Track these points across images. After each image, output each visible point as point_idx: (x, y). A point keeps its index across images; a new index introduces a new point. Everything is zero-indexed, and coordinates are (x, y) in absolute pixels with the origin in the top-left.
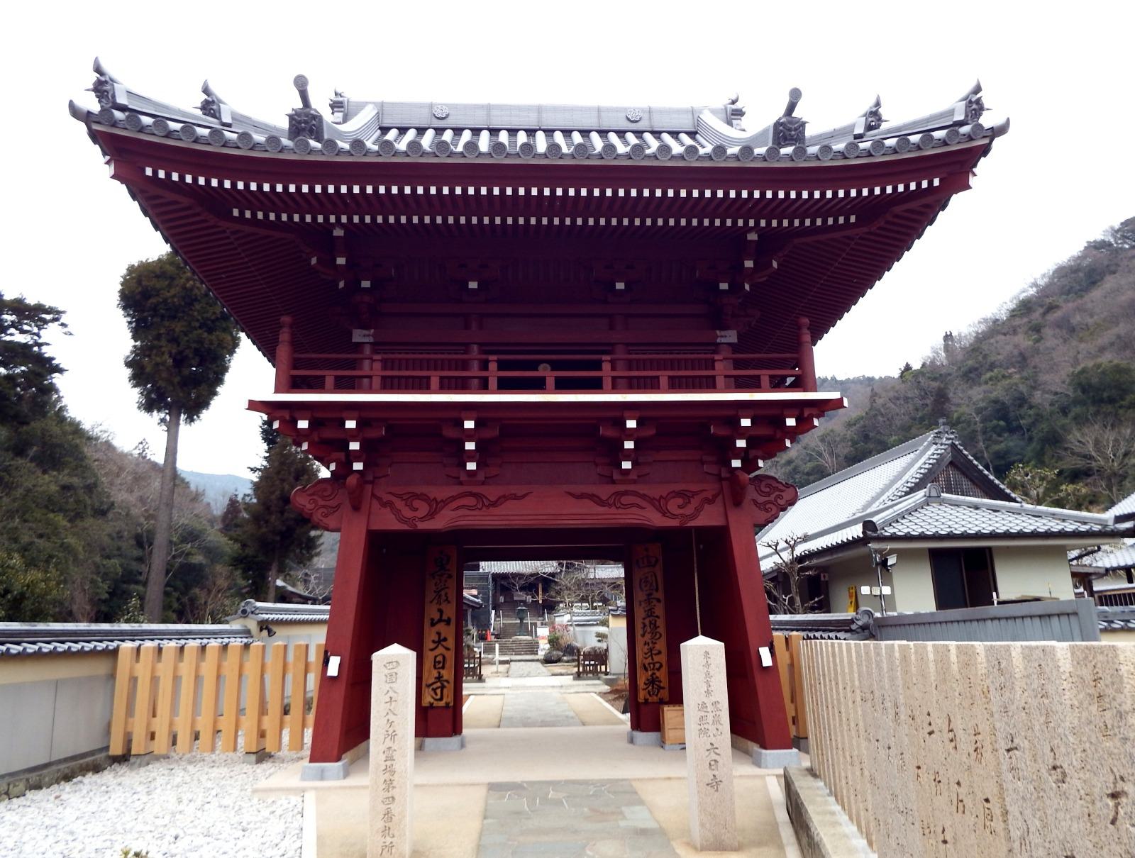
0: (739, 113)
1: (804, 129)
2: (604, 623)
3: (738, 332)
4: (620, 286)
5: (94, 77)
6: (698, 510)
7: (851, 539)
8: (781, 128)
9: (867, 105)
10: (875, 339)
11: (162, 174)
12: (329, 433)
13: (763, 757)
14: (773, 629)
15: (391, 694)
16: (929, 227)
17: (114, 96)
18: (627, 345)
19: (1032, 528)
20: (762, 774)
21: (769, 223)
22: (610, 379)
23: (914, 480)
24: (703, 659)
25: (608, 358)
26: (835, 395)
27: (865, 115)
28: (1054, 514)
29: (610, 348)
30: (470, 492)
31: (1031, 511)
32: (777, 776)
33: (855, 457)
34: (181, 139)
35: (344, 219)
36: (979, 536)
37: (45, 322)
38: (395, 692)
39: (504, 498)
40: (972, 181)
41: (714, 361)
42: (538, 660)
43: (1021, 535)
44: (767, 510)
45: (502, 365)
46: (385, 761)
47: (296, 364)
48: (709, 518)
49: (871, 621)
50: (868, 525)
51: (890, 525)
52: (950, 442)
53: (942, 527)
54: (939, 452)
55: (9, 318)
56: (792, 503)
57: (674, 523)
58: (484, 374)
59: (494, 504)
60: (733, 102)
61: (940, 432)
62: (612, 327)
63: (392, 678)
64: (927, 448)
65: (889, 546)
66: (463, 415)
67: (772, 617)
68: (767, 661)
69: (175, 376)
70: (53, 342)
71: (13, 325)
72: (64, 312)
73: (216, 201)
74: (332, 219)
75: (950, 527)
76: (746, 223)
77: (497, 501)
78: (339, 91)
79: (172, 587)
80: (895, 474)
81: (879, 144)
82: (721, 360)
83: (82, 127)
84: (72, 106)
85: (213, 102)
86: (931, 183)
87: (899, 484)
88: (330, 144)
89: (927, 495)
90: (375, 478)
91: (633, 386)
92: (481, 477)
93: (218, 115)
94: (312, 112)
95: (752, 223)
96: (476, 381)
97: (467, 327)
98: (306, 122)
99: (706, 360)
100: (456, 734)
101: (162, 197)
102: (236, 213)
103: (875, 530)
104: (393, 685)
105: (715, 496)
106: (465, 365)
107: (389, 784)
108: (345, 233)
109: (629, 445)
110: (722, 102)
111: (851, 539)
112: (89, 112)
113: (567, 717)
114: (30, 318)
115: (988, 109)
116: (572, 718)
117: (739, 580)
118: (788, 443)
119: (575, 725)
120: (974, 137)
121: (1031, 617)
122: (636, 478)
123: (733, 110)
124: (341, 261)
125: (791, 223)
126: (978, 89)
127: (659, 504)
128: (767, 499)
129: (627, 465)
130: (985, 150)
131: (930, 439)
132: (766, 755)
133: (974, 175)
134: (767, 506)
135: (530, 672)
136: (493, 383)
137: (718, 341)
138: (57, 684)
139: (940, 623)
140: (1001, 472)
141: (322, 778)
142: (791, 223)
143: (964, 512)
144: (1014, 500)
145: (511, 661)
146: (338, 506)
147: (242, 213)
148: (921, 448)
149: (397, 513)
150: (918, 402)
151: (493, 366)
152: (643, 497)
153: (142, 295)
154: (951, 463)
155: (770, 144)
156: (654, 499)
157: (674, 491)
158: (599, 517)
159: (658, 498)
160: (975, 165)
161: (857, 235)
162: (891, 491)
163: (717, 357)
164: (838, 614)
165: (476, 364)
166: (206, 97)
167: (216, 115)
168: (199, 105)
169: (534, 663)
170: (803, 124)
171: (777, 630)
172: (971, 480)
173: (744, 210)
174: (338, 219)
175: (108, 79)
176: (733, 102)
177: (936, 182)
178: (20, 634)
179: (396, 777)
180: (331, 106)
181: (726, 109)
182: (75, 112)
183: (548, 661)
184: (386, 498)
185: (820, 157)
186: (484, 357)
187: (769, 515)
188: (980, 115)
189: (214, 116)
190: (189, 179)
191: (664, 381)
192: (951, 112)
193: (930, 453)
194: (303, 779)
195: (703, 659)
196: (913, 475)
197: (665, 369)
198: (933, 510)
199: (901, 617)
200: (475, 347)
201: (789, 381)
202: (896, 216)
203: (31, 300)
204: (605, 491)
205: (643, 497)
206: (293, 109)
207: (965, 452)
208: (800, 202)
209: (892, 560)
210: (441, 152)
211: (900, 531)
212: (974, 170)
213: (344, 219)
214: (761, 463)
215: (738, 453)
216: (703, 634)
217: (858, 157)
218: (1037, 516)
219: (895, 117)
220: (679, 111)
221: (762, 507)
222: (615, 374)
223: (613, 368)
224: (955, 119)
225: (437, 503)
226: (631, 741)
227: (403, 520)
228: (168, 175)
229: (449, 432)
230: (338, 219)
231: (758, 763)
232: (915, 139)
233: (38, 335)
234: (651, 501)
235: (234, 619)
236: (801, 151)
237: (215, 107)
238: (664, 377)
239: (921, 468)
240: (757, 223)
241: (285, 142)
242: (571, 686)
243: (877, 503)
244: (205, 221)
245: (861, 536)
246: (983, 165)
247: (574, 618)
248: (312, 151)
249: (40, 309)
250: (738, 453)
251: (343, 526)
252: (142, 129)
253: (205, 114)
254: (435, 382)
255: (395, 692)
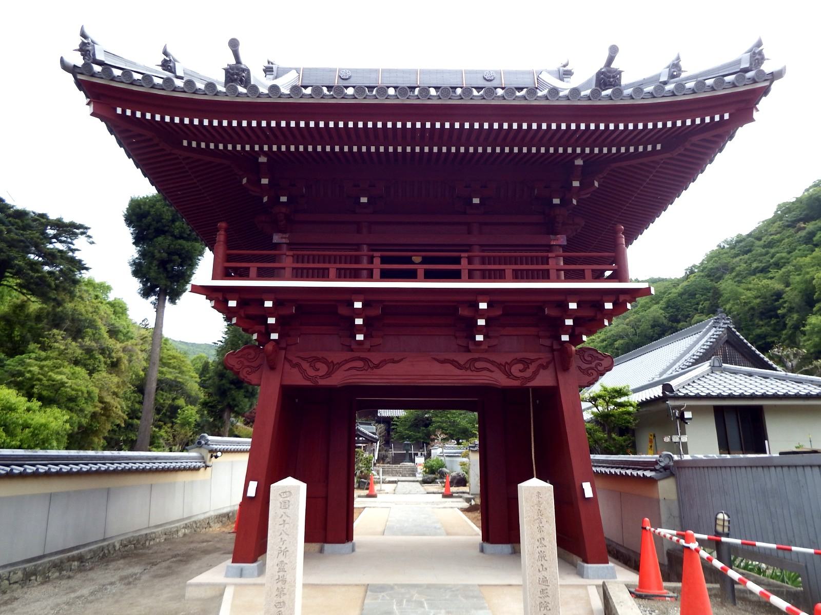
0: (568, 73)
1: (620, 77)
2: (466, 456)
3: (567, 237)
4: (476, 201)
5: (79, 40)
6: (535, 374)
7: (649, 399)
8: (602, 76)
9: (670, 60)
10: (665, 250)
11: (129, 113)
12: (252, 311)
13: (585, 569)
14: (593, 466)
15: (284, 518)
16: (719, 154)
17: (94, 55)
18: (481, 246)
19: (796, 391)
20: (585, 583)
21: (592, 151)
22: (467, 271)
23: (698, 354)
24: (535, 496)
25: (466, 255)
26: (645, 285)
27: (668, 67)
28: (812, 381)
29: (468, 248)
30: (359, 357)
31: (795, 379)
32: (597, 586)
33: (653, 337)
34: (142, 86)
35: (266, 148)
36: (753, 397)
37: (76, 235)
38: (288, 516)
39: (384, 362)
40: (755, 115)
41: (548, 258)
42: (417, 481)
43: (786, 397)
44: (589, 375)
45: (384, 260)
46: (278, 572)
47: (229, 258)
48: (544, 379)
49: (672, 464)
50: (667, 387)
51: (684, 387)
52: (726, 326)
53: (724, 389)
54: (718, 333)
55: (51, 232)
56: (609, 369)
57: (516, 383)
58: (370, 266)
59: (377, 366)
60: (564, 66)
61: (718, 319)
62: (469, 232)
63: (285, 505)
64: (709, 330)
65: (686, 403)
66: (353, 297)
67: (592, 456)
68: (589, 493)
69: (162, 276)
70: (82, 249)
71: (55, 236)
72: (89, 228)
73: (173, 133)
74: (257, 148)
75: (730, 389)
76: (574, 150)
77: (379, 364)
78: (271, 60)
79: (162, 421)
80: (685, 349)
81: (680, 86)
82: (554, 257)
83: (70, 77)
84: (62, 61)
85: (170, 60)
86: (722, 117)
87: (687, 357)
88: (254, 89)
89: (712, 365)
90: (287, 345)
91: (485, 277)
92: (367, 345)
93: (173, 70)
94: (243, 66)
95: (579, 150)
96: (365, 273)
97: (359, 231)
98: (237, 74)
99: (542, 257)
100: (348, 541)
101: (131, 131)
102: (185, 143)
103: (672, 391)
104: (287, 511)
105: (548, 363)
106: (357, 260)
107: (281, 592)
108: (268, 160)
109: (481, 322)
110: (556, 65)
111: (645, 400)
112: (75, 66)
113: (435, 528)
114: (65, 232)
115: (768, 59)
116: (439, 528)
117: (567, 428)
118: (606, 323)
119: (441, 535)
120: (757, 80)
121: (811, 466)
122: (487, 347)
123: (564, 71)
124: (265, 181)
125: (610, 150)
126: (759, 44)
127: (505, 369)
128: (589, 366)
129: (479, 338)
130: (765, 91)
131: (710, 324)
132: (588, 567)
133: (757, 110)
134: (589, 372)
135: (410, 491)
136: (377, 273)
137: (552, 243)
138: (51, 496)
139: (730, 467)
140: (764, 350)
141: (241, 576)
142: (610, 150)
143: (741, 378)
144: (775, 369)
145: (399, 481)
146: (259, 367)
147: (190, 144)
148: (704, 330)
149: (303, 372)
150: (677, 310)
151: (377, 261)
152: (493, 363)
153: (139, 217)
154: (727, 342)
155: (594, 87)
156: (501, 364)
157: (516, 359)
158: (461, 378)
159: (504, 364)
160: (757, 103)
161: (662, 159)
162: (681, 362)
163: (550, 255)
164: (644, 456)
165: (365, 259)
166: (165, 57)
167: (172, 70)
168: (160, 64)
169: (414, 483)
170: (620, 73)
171: (595, 466)
172: (742, 355)
173: (573, 140)
174: (261, 148)
175: (90, 41)
176: (564, 66)
177: (726, 116)
178: (4, 458)
179: (287, 586)
180: (264, 70)
181: (559, 71)
182: (65, 66)
183: (424, 482)
184: (295, 360)
185: (634, 97)
186: (371, 253)
187: (591, 378)
188: (762, 63)
189: (170, 71)
190: (148, 116)
191: (509, 273)
192: (738, 62)
193: (710, 334)
194: (227, 576)
195: (535, 496)
196: (698, 350)
197: (510, 264)
198: (716, 376)
199: (695, 461)
200: (365, 247)
201: (608, 273)
202: (693, 145)
203: (67, 220)
204: (462, 358)
205: (493, 363)
206: (228, 65)
207: (738, 333)
208: (617, 133)
209: (688, 415)
210: (338, 94)
211: (724, 392)
212: (757, 106)
213: (266, 148)
214: (585, 338)
215: (566, 330)
216: (539, 477)
217: (663, 96)
218: (799, 382)
219: (692, 68)
220: (523, 73)
221: (585, 372)
222: (471, 267)
223: (470, 263)
224: (742, 67)
225: (334, 365)
226: (482, 550)
227: (307, 378)
228: (133, 113)
229: (342, 311)
230: (261, 148)
231: (581, 574)
232: (709, 82)
233: (72, 243)
234: (499, 366)
235: (192, 449)
236: (618, 92)
237: (171, 65)
238: (509, 269)
239: (704, 345)
240: (583, 151)
241: (221, 88)
242: (441, 503)
243: (670, 371)
244: (163, 150)
245: (661, 395)
246: (764, 104)
247: (445, 451)
248: (239, 95)
249: (73, 225)
250: (566, 330)
251: (262, 383)
252: (113, 79)
253: (164, 70)
254: (333, 272)
255: (288, 516)
